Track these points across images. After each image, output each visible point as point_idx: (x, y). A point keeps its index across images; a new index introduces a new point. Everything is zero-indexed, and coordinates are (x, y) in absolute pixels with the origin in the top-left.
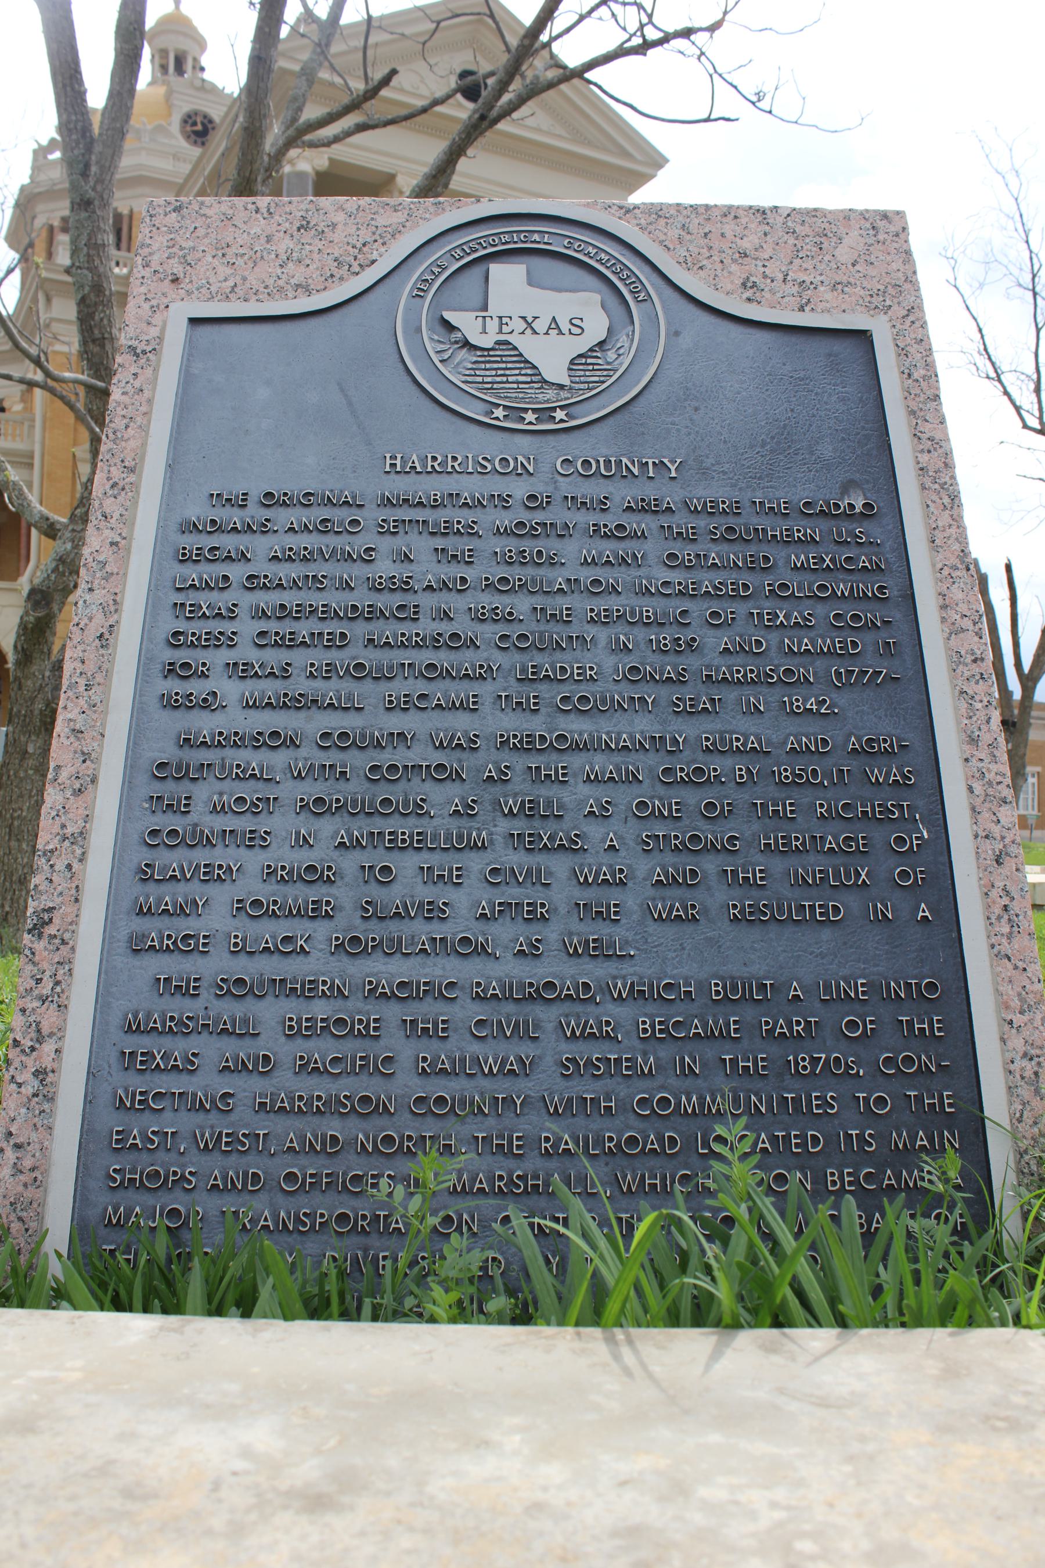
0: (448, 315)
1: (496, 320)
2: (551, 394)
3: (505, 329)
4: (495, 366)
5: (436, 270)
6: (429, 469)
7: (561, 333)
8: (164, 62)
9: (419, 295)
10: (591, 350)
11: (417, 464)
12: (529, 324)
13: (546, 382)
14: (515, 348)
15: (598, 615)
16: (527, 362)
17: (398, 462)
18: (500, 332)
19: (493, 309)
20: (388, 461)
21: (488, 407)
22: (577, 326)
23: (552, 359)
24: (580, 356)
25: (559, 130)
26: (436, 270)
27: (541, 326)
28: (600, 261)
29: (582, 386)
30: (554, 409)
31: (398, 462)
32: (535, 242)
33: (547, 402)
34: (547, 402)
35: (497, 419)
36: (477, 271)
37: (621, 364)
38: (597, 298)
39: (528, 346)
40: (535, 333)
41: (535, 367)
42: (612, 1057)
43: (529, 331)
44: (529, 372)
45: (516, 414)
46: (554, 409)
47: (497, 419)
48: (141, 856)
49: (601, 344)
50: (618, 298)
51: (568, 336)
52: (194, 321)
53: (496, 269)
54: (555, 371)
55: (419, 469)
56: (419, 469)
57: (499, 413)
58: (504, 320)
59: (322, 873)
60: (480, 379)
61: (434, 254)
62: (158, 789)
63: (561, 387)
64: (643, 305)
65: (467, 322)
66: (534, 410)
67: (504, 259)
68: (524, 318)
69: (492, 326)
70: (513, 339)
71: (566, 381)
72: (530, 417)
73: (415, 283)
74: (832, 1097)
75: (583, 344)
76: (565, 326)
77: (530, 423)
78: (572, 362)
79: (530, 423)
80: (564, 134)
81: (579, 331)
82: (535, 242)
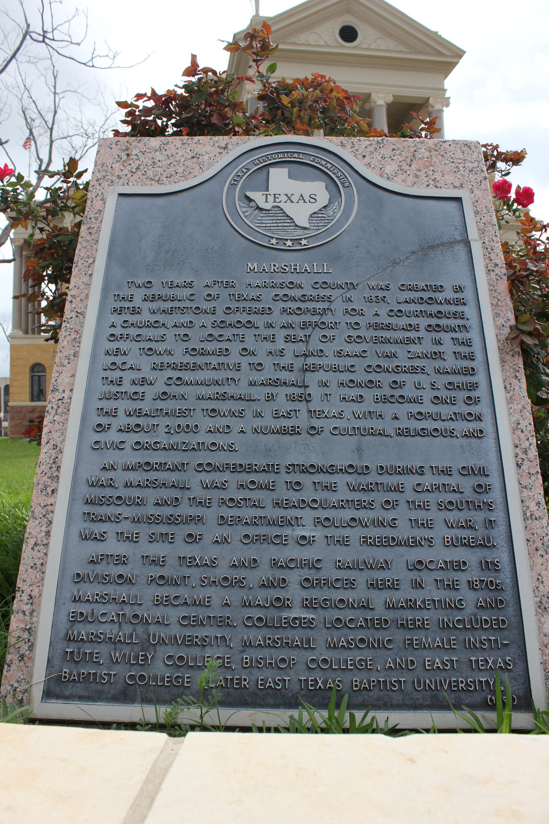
0: (248, 194)
1: (273, 196)
2: (300, 232)
3: (277, 200)
4: (272, 218)
5: (244, 171)
6: (272, 271)
7: (305, 202)
8: (7, 397)
9: (233, 185)
10: (320, 210)
11: (308, 268)
12: (289, 198)
13: (297, 226)
14: (282, 210)
15: (408, 369)
16: (288, 216)
17: (298, 267)
18: (275, 202)
19: (272, 190)
20: (293, 267)
21: (268, 238)
22: (313, 198)
23: (301, 214)
24: (315, 213)
25: (400, 48)
26: (244, 171)
27: (295, 198)
28: (327, 168)
29: (315, 228)
30: (301, 239)
31: (298, 267)
32: (295, 158)
33: (297, 236)
34: (297, 236)
35: (272, 244)
36: (264, 172)
37: (335, 217)
38: (323, 185)
39: (288, 208)
40: (292, 202)
41: (292, 219)
42: (402, 680)
43: (289, 201)
44: (289, 221)
45: (282, 242)
46: (301, 239)
47: (272, 244)
48: (73, 589)
49: (325, 207)
50: (333, 185)
51: (308, 204)
52: (120, 195)
53: (273, 171)
54: (302, 220)
55: (309, 271)
56: (309, 271)
57: (274, 241)
58: (277, 196)
59: (143, 445)
60: (264, 225)
61: (242, 163)
62: (87, 509)
63: (305, 228)
64: (346, 189)
65: (258, 197)
66: (291, 240)
67: (280, 165)
68: (286, 195)
69: (271, 199)
70: (281, 205)
71: (307, 226)
72: (289, 243)
73: (233, 177)
74: (509, 660)
75: (316, 207)
76: (307, 199)
77: (305, 245)
78: (311, 216)
79: (289, 246)
80: (405, 50)
81: (314, 201)
82: (295, 158)
